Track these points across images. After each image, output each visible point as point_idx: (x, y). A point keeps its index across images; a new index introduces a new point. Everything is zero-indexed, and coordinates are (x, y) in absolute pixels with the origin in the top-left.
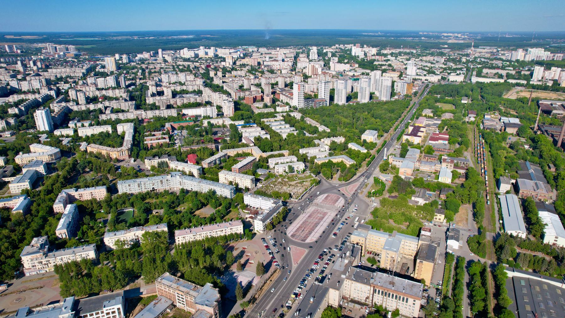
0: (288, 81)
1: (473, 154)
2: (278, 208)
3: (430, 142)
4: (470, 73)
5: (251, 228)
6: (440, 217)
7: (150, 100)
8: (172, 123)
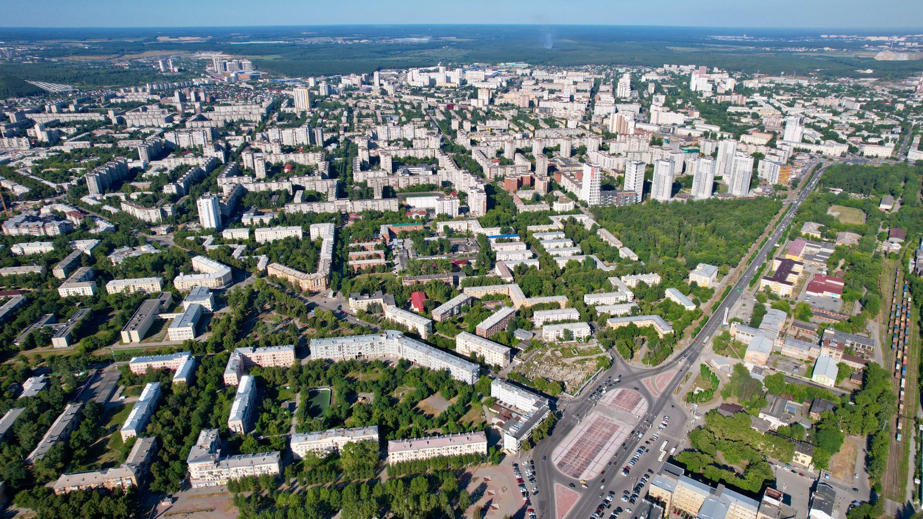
0: (577, 143)
1: (885, 327)
2: (542, 412)
3: (808, 293)
4: (907, 138)
5: (499, 443)
6: (804, 459)
7: (359, 177)
8: (390, 226)
